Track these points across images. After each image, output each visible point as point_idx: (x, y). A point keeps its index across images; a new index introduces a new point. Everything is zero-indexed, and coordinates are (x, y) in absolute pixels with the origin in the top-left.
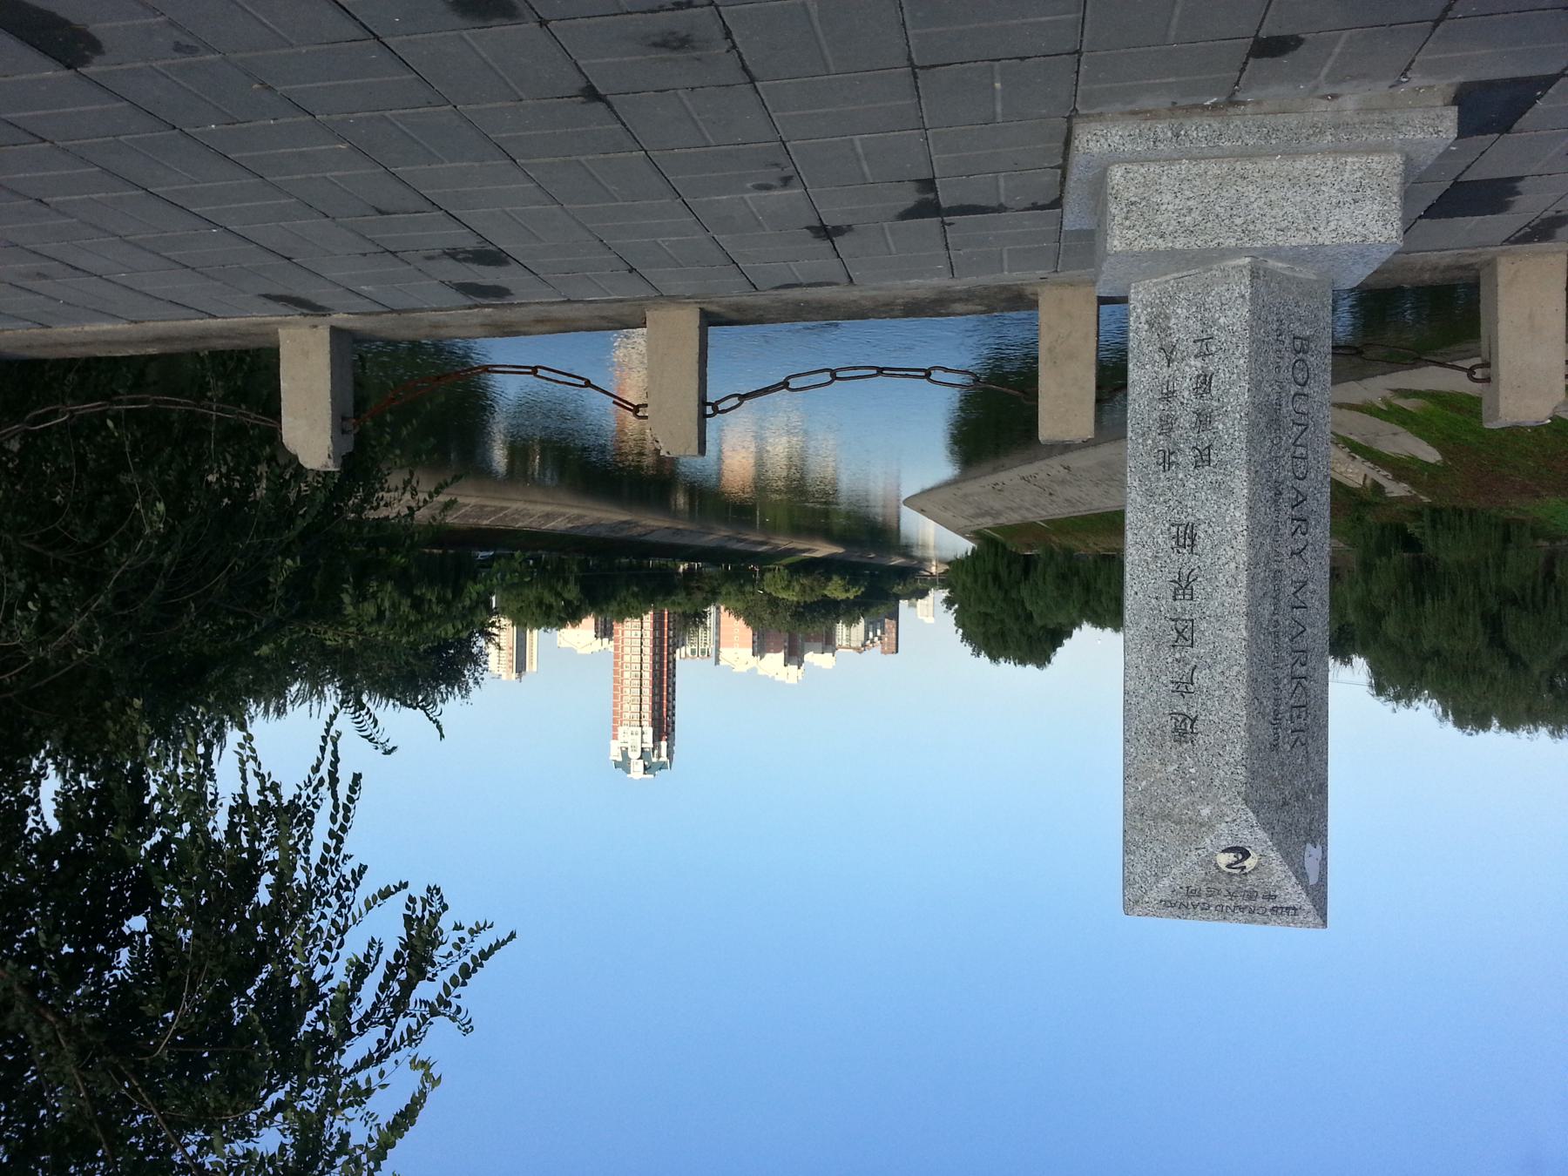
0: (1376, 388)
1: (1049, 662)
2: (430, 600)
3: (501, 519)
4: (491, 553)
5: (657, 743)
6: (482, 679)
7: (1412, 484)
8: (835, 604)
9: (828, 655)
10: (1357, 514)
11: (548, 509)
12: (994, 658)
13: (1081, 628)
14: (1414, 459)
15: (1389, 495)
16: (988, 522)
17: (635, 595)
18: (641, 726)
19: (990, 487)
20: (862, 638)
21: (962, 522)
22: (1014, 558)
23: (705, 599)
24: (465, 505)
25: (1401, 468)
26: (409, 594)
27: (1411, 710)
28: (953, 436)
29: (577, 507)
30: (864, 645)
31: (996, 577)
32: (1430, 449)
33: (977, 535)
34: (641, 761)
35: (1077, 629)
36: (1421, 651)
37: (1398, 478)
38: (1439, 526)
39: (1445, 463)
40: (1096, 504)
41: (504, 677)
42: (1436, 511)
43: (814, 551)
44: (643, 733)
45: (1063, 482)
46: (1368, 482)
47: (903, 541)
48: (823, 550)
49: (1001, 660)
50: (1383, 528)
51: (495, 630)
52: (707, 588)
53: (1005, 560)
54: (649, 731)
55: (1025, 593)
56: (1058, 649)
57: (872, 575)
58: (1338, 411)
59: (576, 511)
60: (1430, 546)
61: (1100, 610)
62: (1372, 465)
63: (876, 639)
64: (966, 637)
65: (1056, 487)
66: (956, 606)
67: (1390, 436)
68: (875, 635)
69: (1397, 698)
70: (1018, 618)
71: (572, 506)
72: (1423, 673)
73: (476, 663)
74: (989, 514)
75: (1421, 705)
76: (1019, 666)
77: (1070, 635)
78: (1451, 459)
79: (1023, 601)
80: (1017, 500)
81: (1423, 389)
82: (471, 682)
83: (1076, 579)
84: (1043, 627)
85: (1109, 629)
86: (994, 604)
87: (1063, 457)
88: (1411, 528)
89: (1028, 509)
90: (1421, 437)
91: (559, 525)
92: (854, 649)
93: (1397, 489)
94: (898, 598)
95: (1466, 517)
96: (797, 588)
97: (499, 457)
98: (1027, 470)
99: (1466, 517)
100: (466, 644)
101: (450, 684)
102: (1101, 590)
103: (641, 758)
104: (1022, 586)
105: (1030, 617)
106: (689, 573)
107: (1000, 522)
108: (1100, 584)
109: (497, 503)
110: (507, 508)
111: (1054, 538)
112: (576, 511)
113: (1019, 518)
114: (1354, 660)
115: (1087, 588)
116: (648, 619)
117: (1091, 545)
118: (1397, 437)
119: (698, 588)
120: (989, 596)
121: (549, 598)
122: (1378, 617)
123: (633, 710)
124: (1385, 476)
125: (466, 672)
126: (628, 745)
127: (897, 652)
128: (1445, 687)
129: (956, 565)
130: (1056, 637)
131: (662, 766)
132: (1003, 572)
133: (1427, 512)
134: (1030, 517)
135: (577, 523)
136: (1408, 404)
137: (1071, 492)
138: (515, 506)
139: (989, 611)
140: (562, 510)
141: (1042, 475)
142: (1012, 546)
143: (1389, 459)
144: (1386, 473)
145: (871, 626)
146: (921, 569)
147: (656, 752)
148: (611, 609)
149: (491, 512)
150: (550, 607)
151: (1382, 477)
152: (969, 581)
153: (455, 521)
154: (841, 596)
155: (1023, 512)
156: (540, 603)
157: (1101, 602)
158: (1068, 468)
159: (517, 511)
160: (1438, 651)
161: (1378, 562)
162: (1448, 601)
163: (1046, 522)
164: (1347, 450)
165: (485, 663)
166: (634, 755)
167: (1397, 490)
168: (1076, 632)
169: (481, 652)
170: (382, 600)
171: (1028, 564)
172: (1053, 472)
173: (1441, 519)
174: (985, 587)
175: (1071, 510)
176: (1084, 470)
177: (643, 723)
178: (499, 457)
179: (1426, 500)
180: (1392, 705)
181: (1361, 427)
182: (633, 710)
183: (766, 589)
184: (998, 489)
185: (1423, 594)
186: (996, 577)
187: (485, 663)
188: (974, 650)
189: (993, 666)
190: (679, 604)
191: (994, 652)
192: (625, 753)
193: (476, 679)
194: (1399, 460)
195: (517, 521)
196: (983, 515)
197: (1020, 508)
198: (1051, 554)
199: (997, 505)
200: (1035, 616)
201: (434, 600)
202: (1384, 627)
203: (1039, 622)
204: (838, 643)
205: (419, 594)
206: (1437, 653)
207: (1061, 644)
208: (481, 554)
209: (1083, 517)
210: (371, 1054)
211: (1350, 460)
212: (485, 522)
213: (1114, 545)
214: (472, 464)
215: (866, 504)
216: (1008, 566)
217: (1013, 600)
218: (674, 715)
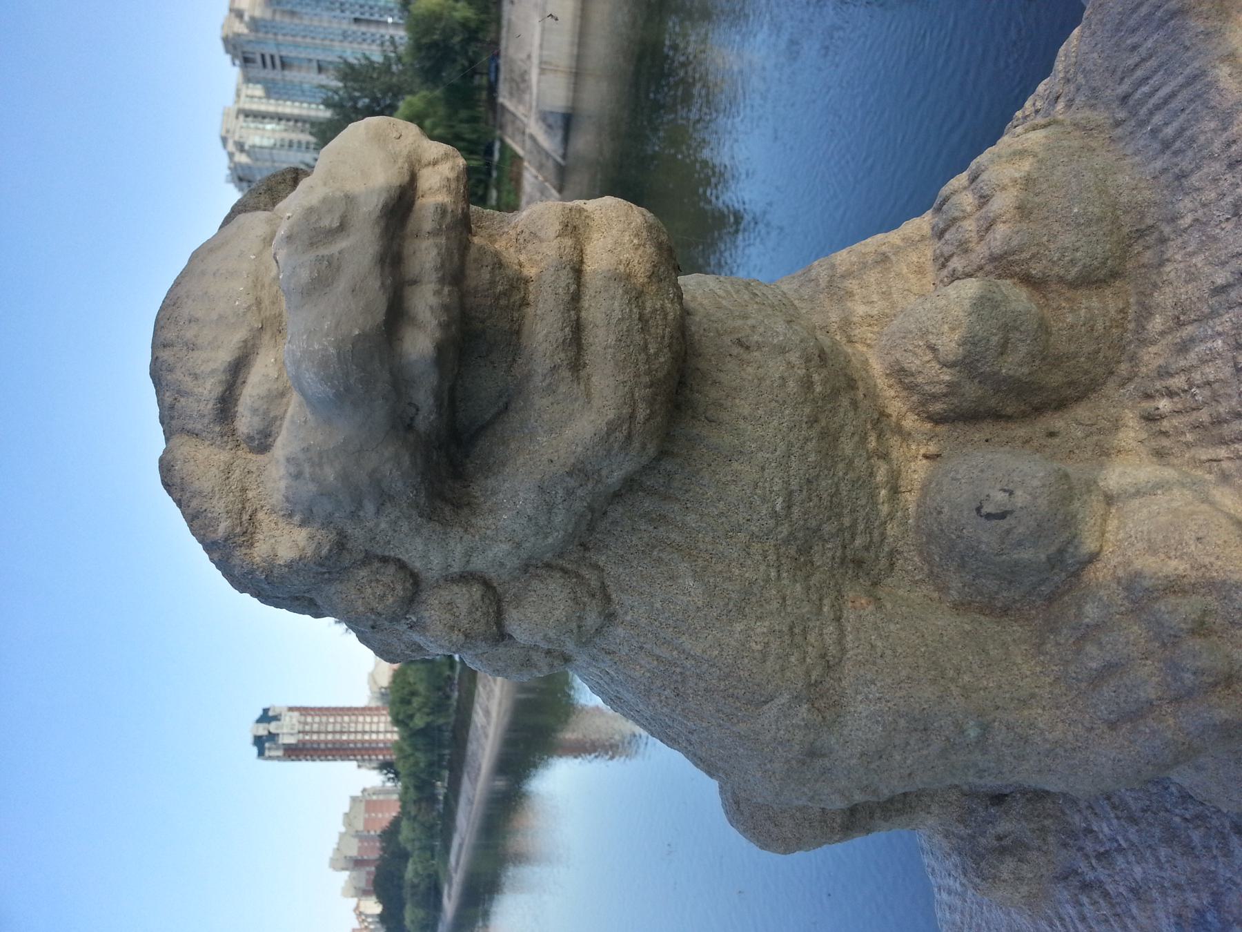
11: (494, 714)
28: (385, 206)
30: (361, 914)
43: (449, 897)
44: (292, 734)
63: (366, 924)
68: (370, 923)
91: (478, 718)
103: (270, 733)
131: (261, 754)
135: (480, 732)
150: (409, 703)
156: (414, 694)
159: (492, 691)
166: (273, 727)
192: (276, 718)
210: (275, 145)
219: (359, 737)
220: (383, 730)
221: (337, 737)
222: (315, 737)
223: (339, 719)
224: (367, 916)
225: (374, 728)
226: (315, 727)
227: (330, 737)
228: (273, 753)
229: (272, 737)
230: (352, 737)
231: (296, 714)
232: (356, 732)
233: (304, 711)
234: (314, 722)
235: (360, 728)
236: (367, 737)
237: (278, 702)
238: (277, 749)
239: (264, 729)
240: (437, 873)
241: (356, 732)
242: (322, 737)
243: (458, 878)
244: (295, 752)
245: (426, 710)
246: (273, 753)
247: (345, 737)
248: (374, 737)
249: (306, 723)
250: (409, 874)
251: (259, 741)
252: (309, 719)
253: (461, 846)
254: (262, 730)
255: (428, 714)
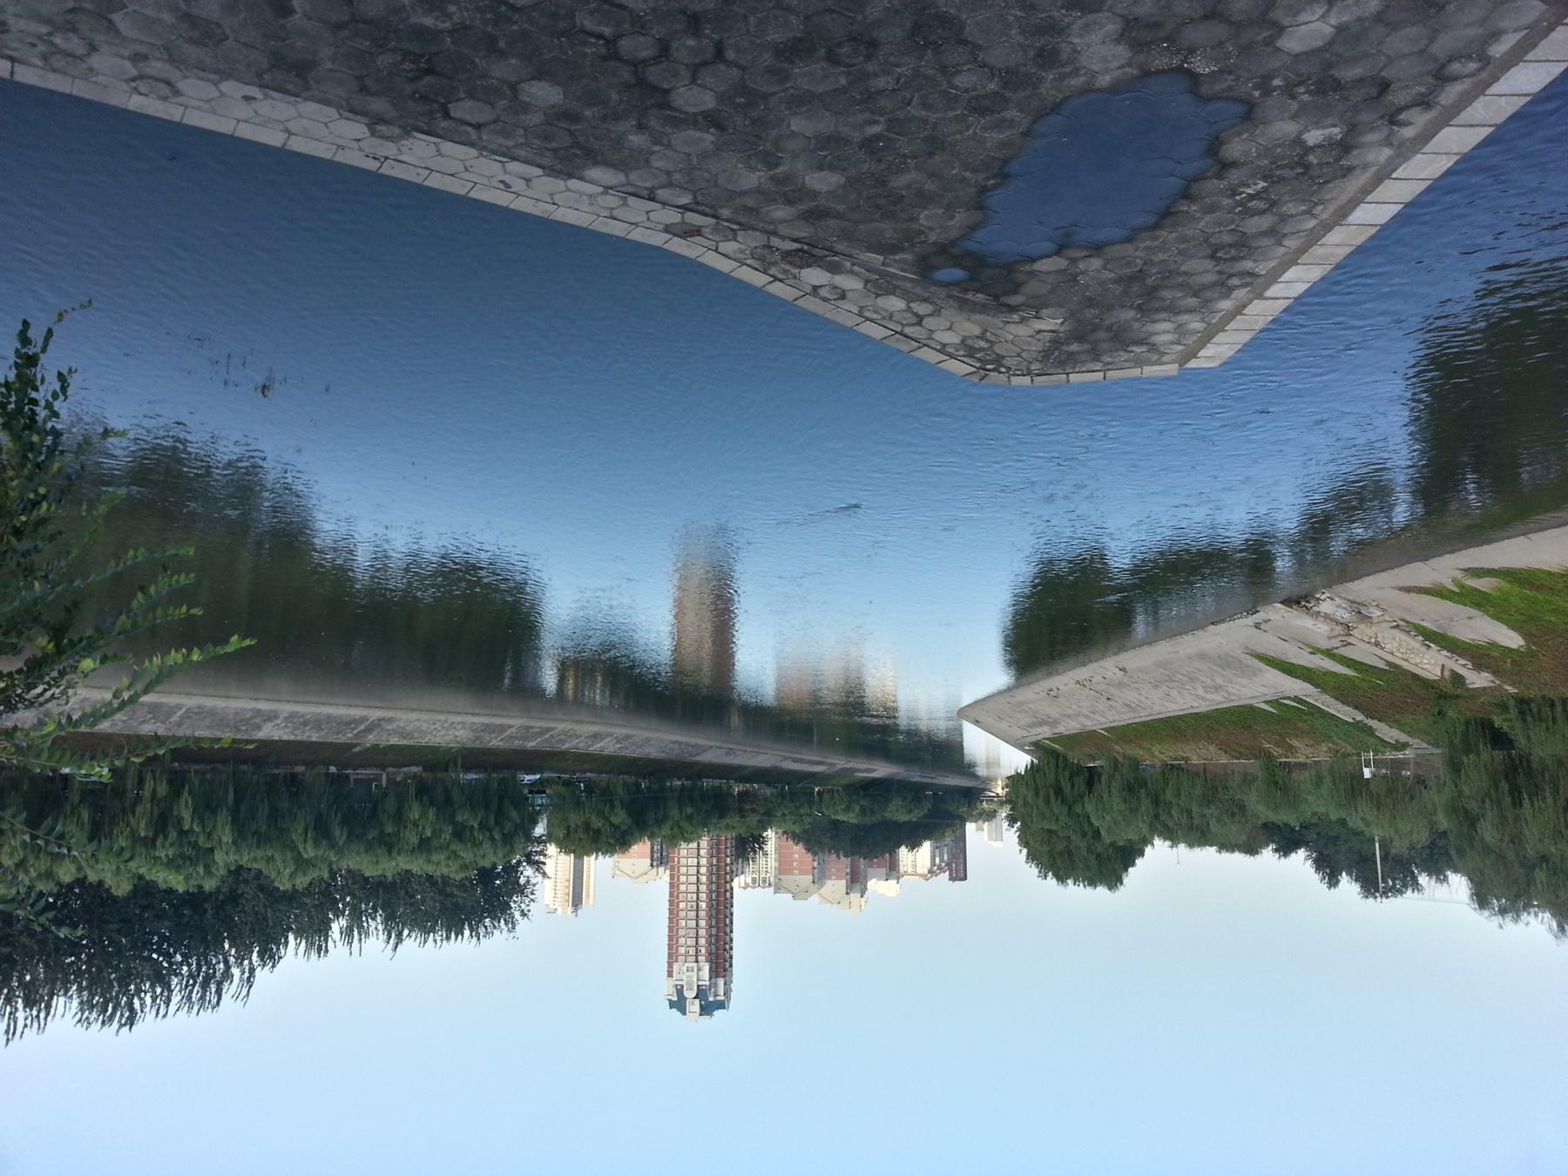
0: (1445, 568)
1: (1121, 883)
2: (472, 826)
3: (547, 740)
4: (538, 776)
5: (713, 980)
6: (529, 911)
7: (1495, 673)
8: (898, 825)
9: (892, 882)
10: (1438, 708)
11: (595, 729)
12: (1061, 878)
13: (1153, 845)
14: (1493, 645)
15: (1471, 686)
16: (1044, 732)
17: (689, 818)
18: (697, 962)
19: (1044, 694)
20: (928, 864)
21: (1019, 733)
22: (1078, 770)
23: (760, 821)
24: (511, 727)
25: (1481, 656)
26: (452, 820)
27: (1521, 925)
29: (625, 726)
30: (930, 871)
31: (1059, 791)
32: (1511, 633)
33: (1037, 748)
34: (697, 1001)
35: (1149, 846)
36: (1525, 857)
37: (1478, 667)
38: (1529, 719)
39: (1529, 648)
40: (1157, 708)
41: (559, 912)
42: (1523, 703)
43: (874, 771)
44: (699, 970)
45: (1120, 685)
46: (1447, 673)
47: (967, 758)
48: (882, 770)
49: (1070, 882)
50: (1467, 723)
51: (542, 858)
52: (762, 811)
53: (1067, 774)
54: (706, 968)
55: (1089, 808)
56: (1130, 869)
57: (935, 794)
58: (1406, 595)
59: (624, 731)
60: (1521, 741)
61: (1170, 824)
62: (1449, 654)
64: (1032, 857)
65: (1113, 690)
66: (1019, 823)
67: (1466, 621)
69: (1503, 911)
70: (1084, 835)
71: (619, 726)
72: (1530, 882)
73: (522, 892)
74: (1047, 723)
75: (1531, 919)
76: (1089, 888)
77: (1142, 854)
78: (1535, 643)
79: (1089, 817)
80: (1074, 707)
81: (1496, 568)
82: (517, 915)
83: (1143, 791)
84: (1113, 844)
85: (1183, 845)
86: (1057, 820)
87: (1116, 658)
88: (1498, 722)
89: (1087, 716)
90: (1498, 619)
91: (608, 747)
92: (920, 875)
93: (1479, 680)
94: (963, 821)
95: (1559, 708)
96: (857, 808)
97: (549, 679)
98: (1082, 673)
99: (1559, 708)
100: (512, 871)
101: (495, 918)
102: (1171, 803)
104: (1086, 799)
105: (1097, 834)
106: (743, 795)
107: (1057, 731)
108: (1169, 796)
109: (544, 724)
110: (556, 728)
111: (1116, 747)
112: (624, 731)
113: (1078, 726)
114: (1450, 878)
115: (1156, 801)
116: (704, 843)
117: (1157, 753)
118: (1472, 621)
119: (753, 810)
120: (1052, 811)
121: (597, 823)
122: (1471, 820)
123: (688, 943)
124: (1464, 666)
125: (512, 904)
126: (683, 983)
127: (966, 879)
128: (1558, 897)
129: (1014, 781)
130: (1128, 855)
131: (721, 1005)
132: (1067, 788)
133: (1512, 703)
134: (1090, 725)
136: (1484, 584)
137: (1130, 696)
138: (561, 726)
139: (1054, 827)
140: (611, 730)
141: (1097, 679)
142: (1075, 757)
143: (1467, 646)
144: (1464, 662)
145: (937, 851)
146: (986, 790)
147: (713, 990)
148: (663, 833)
149: (536, 733)
150: (598, 832)
151: (1461, 666)
152: (1030, 796)
153: (501, 743)
154: (903, 817)
155: (1081, 719)
156: (587, 826)
157: (1172, 816)
158: (1123, 670)
159: (564, 732)
160: (1544, 856)
161: (1465, 759)
162: (1550, 800)
163: (1109, 730)
164: (1421, 638)
165: (532, 894)
166: (690, 994)
167: (1479, 680)
168: (1148, 850)
169: (528, 882)
170: (423, 828)
171: (1092, 776)
172: (1109, 675)
173: (1530, 710)
174: (1048, 802)
175: (1132, 715)
176: (1140, 671)
177: (700, 958)
178: (549, 679)
179: (1512, 690)
180: (1497, 920)
181: (1433, 612)
182: (688, 943)
183: (825, 811)
184: (1053, 695)
185: (1520, 793)
186: (1059, 791)
187: (532, 894)
188: (1040, 872)
189: (1061, 888)
190: (733, 827)
191: (1061, 873)
192: (680, 991)
193: (522, 911)
194: (1478, 646)
195: (563, 742)
196: (1041, 724)
197: (1078, 715)
198: (1116, 765)
199: (1054, 714)
200: (1102, 832)
201: (476, 826)
202: (1479, 831)
203: (1107, 838)
204: (902, 869)
205: (460, 820)
206: (1544, 858)
207: (1133, 864)
208: (528, 778)
209: (1143, 724)
211: (1424, 649)
212: (534, 744)
213: (1181, 753)
214: (526, 692)
215: (893, 699)
216: (1071, 778)
217: (1079, 815)
218: (731, 949)
219: (703, 888)
220: (694, 855)
221: (702, 914)
222: (702, 941)
223: (682, 914)
224: (933, 864)
225: (693, 870)
226: (691, 942)
227: (703, 923)
228: (721, 991)
229: (701, 994)
230: (703, 896)
231: (676, 967)
232: (698, 892)
233: (672, 957)
234: (685, 943)
235: (693, 888)
236: (704, 879)
237: (666, 989)
238: (716, 985)
239: (693, 1004)
240: (847, 787)
241: (698, 892)
242: (702, 932)
243: (840, 762)
244: (720, 962)
245: (607, 809)
246: (721, 991)
247: (703, 905)
248: (703, 870)
249: (687, 954)
250: (851, 818)
251: (707, 1009)
252: (682, 950)
253: (795, 760)
254: (695, 1006)
255: (613, 807)
